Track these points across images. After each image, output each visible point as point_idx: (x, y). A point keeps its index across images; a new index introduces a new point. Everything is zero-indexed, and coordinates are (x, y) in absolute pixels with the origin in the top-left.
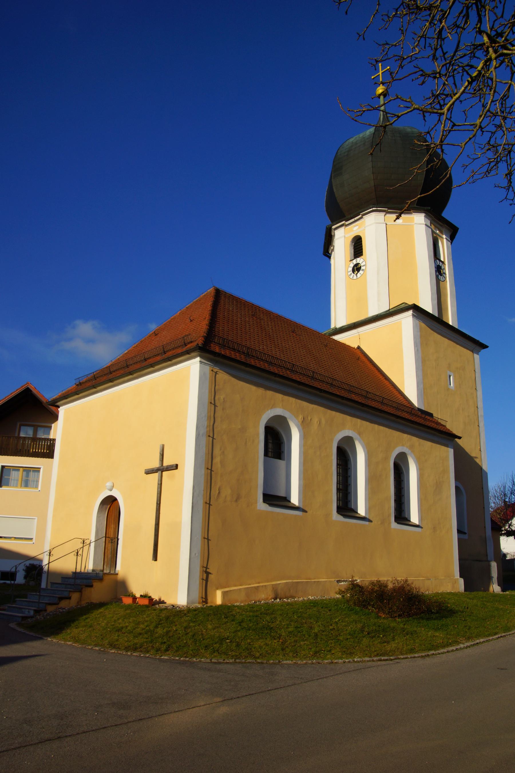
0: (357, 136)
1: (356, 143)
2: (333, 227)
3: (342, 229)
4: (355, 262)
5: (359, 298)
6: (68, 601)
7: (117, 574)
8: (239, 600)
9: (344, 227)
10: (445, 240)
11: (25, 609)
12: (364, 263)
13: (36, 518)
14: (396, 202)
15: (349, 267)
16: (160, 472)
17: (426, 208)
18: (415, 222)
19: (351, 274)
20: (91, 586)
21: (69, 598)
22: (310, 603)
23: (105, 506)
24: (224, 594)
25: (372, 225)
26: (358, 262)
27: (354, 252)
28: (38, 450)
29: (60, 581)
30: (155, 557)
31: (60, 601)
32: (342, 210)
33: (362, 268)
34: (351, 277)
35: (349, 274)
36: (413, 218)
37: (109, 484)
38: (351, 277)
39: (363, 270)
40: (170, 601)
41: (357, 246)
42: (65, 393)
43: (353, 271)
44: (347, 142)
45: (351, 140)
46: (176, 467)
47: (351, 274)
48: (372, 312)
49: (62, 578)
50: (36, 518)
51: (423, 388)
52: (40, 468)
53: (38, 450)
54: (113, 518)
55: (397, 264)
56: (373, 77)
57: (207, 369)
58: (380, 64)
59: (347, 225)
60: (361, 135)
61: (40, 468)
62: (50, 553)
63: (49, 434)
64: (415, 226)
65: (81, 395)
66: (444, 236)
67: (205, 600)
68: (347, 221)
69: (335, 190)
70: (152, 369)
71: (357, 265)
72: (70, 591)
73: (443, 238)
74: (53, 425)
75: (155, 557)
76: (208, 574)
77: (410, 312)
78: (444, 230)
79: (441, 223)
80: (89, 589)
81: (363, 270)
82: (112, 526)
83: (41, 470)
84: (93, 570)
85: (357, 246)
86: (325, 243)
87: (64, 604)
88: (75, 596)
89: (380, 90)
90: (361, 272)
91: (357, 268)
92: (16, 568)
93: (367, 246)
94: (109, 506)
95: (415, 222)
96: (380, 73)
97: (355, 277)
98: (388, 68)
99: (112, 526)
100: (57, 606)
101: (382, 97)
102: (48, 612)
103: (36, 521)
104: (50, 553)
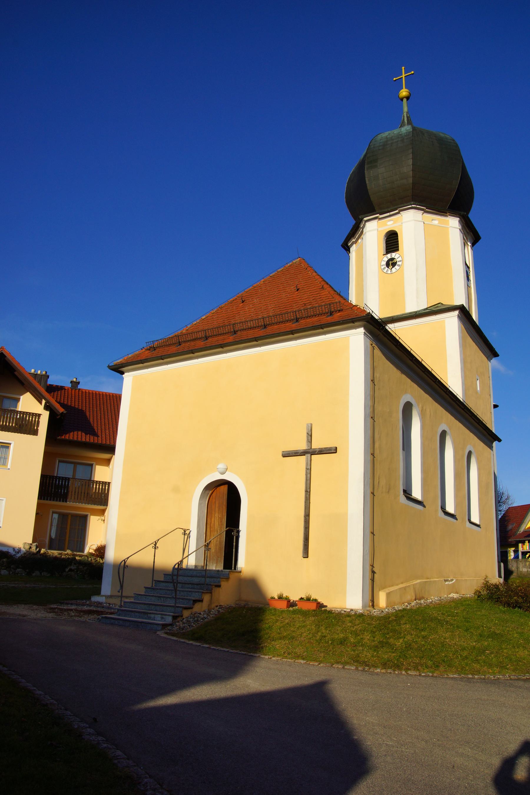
0: (390, 132)
1: (391, 139)
2: (365, 219)
3: (374, 223)
4: (389, 256)
5: (398, 293)
6: (200, 603)
7: (240, 572)
8: (408, 601)
9: (377, 220)
10: (469, 248)
11: (150, 613)
12: (400, 259)
13: (5, 499)
14: (435, 202)
15: (382, 260)
16: (309, 455)
17: (462, 213)
18: (450, 225)
19: (384, 268)
20: (219, 586)
21: (201, 601)
22: (450, 602)
23: (207, 492)
24: (388, 595)
25: (410, 223)
26: (393, 257)
27: (386, 247)
28: (9, 423)
29: (162, 579)
30: (306, 554)
31: (194, 604)
32: (363, 203)
33: (398, 263)
34: (385, 271)
35: (382, 267)
36: (448, 221)
37: (221, 466)
38: (385, 271)
39: (399, 265)
40: (332, 603)
41: (392, 242)
42: (134, 357)
43: (388, 265)
44: (379, 137)
45: (386, 134)
46: (334, 451)
47: (384, 268)
48: (411, 308)
49: (165, 575)
50: (5, 499)
51: (465, 389)
52: (10, 444)
53: (9, 423)
54: (217, 505)
55: (435, 263)
56: (395, 79)
57: (369, 342)
58: (403, 68)
59: (380, 219)
60: (396, 131)
61: (10, 444)
62: (155, 545)
63: (16, 407)
64: (450, 229)
65: (165, 360)
66: (469, 243)
67: (373, 602)
68: (381, 214)
69: (367, 182)
70: (291, 336)
71: (392, 259)
72: (203, 593)
73: (468, 244)
74: (22, 397)
75: (306, 554)
76: (373, 572)
77: (457, 313)
78: (468, 238)
79: (467, 230)
80: (217, 589)
81: (399, 265)
82: (217, 515)
83: (12, 447)
84: (196, 566)
85: (392, 242)
86: (349, 234)
87: (197, 608)
88: (206, 598)
89: (404, 93)
90: (396, 267)
91: (391, 263)
92: (125, 563)
93: (404, 241)
94: (211, 492)
95: (450, 225)
96: (403, 76)
97: (389, 272)
98: (413, 72)
99: (217, 515)
100: (191, 610)
101: (405, 100)
102: (184, 617)
103: (4, 502)
104: (155, 545)
